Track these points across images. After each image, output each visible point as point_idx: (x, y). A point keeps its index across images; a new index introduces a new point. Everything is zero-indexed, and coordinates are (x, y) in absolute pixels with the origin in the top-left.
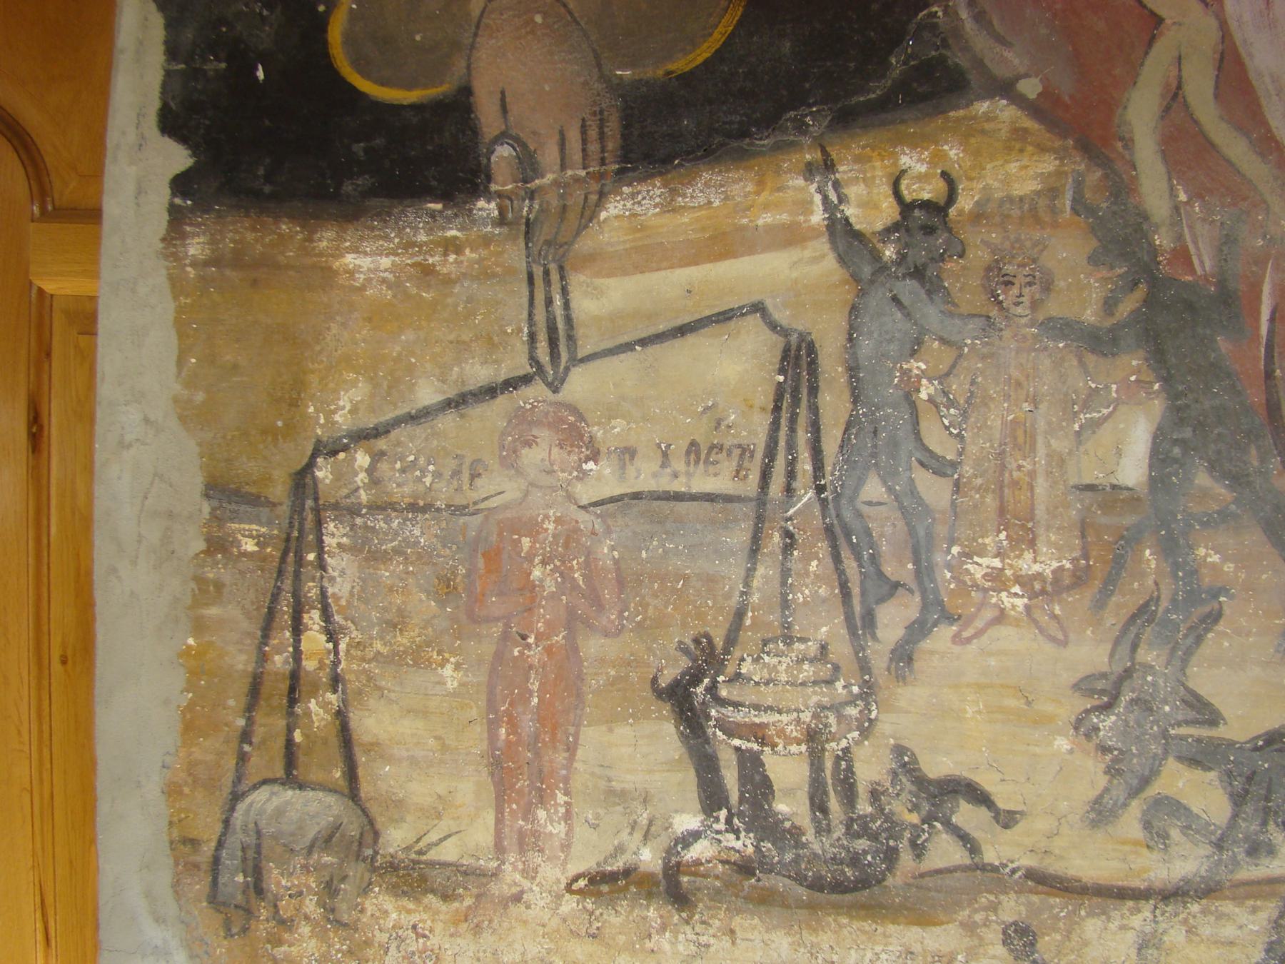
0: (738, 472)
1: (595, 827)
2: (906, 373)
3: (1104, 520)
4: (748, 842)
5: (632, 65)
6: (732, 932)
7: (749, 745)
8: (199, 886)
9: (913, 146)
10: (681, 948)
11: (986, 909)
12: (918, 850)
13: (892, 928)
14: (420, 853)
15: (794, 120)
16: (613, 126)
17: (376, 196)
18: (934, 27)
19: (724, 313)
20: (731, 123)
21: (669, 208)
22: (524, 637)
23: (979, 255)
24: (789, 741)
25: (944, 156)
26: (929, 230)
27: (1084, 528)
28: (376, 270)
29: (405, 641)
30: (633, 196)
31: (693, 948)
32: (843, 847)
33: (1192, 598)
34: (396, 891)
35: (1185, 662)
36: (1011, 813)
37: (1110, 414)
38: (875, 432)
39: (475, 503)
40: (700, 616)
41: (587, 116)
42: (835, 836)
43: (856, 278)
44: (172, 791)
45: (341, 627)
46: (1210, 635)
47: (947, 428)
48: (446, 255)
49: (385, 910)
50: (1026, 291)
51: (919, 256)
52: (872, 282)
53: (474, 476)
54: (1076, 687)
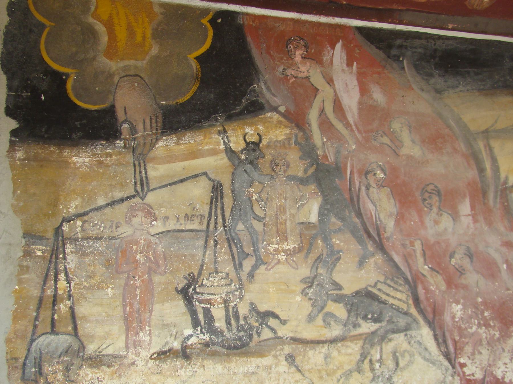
0: (200, 223)
1: (159, 337)
2: (249, 192)
3: (307, 232)
4: (207, 336)
5: (166, 100)
6: (204, 366)
7: (206, 306)
8: (18, 374)
9: (249, 126)
10: (188, 373)
11: (279, 350)
12: (259, 334)
13: (252, 359)
14: (100, 352)
15: (214, 118)
16: (160, 119)
17: (84, 139)
18: (254, 91)
19: (195, 175)
20: (196, 118)
21: (177, 144)
22: (134, 277)
23: (268, 157)
24: (218, 303)
25: (258, 129)
26: (254, 150)
27: (301, 235)
28: (84, 162)
29: (94, 281)
30: (166, 140)
31: (191, 373)
32: (236, 335)
33: (332, 253)
34: (91, 366)
35: (331, 272)
36: (285, 320)
37: (307, 202)
38: (240, 209)
39: (118, 236)
40: (190, 267)
41: (152, 115)
42: (234, 332)
43: (233, 164)
44: (8, 341)
45: (72, 278)
46: (338, 264)
47: (261, 208)
48: (107, 157)
49: (88, 373)
50: (282, 167)
51: (251, 158)
52: (238, 165)
53: (117, 227)
54: (301, 281)
